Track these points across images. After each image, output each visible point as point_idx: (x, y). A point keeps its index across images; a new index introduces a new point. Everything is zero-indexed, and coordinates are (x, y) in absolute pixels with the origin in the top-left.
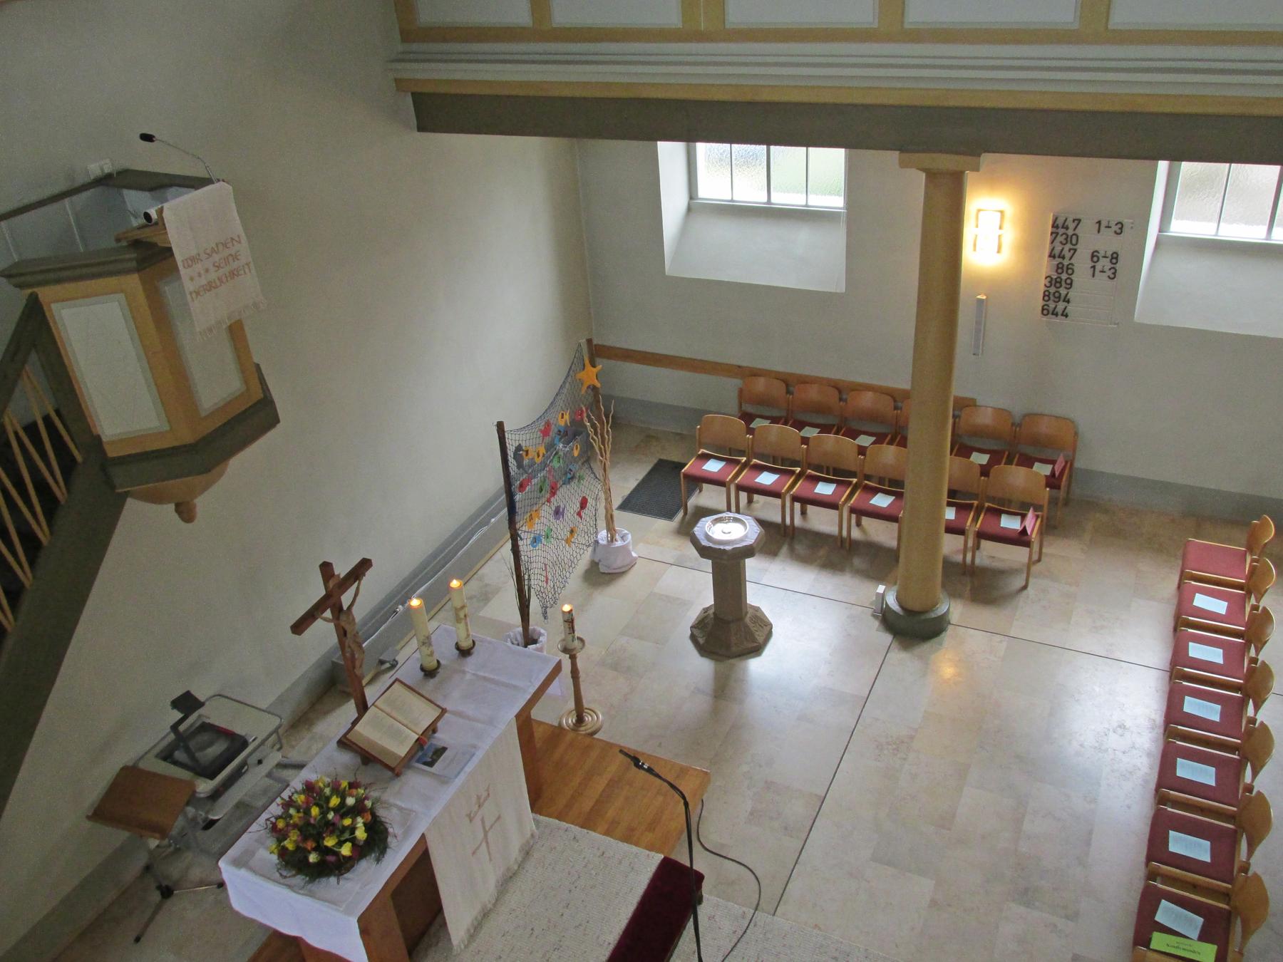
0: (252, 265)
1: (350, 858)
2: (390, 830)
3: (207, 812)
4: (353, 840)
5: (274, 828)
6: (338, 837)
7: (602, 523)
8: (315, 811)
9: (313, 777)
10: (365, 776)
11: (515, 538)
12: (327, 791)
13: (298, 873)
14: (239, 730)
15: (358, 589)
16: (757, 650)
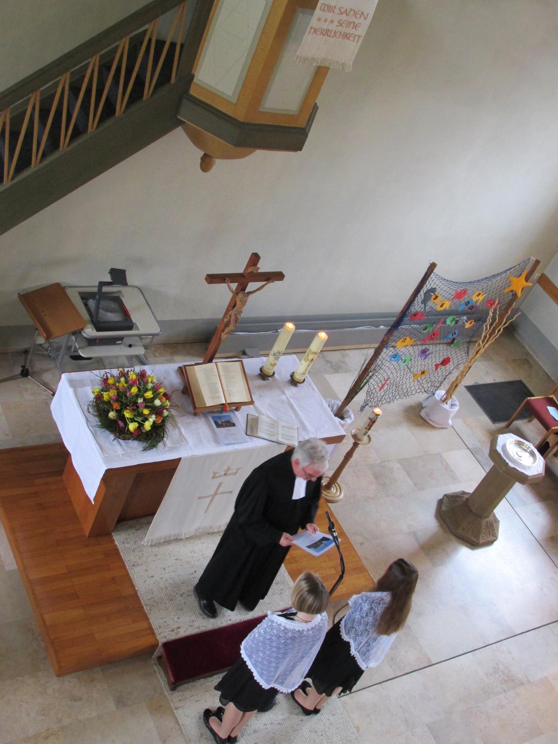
0: (361, 39)
1: (132, 433)
2: (165, 439)
3: (80, 348)
4: (141, 425)
5: (105, 380)
6: (135, 416)
7: (446, 385)
8: (134, 390)
9: (149, 373)
10: (177, 398)
12: (150, 386)
13: (97, 416)
14: (134, 318)
16: (474, 544)
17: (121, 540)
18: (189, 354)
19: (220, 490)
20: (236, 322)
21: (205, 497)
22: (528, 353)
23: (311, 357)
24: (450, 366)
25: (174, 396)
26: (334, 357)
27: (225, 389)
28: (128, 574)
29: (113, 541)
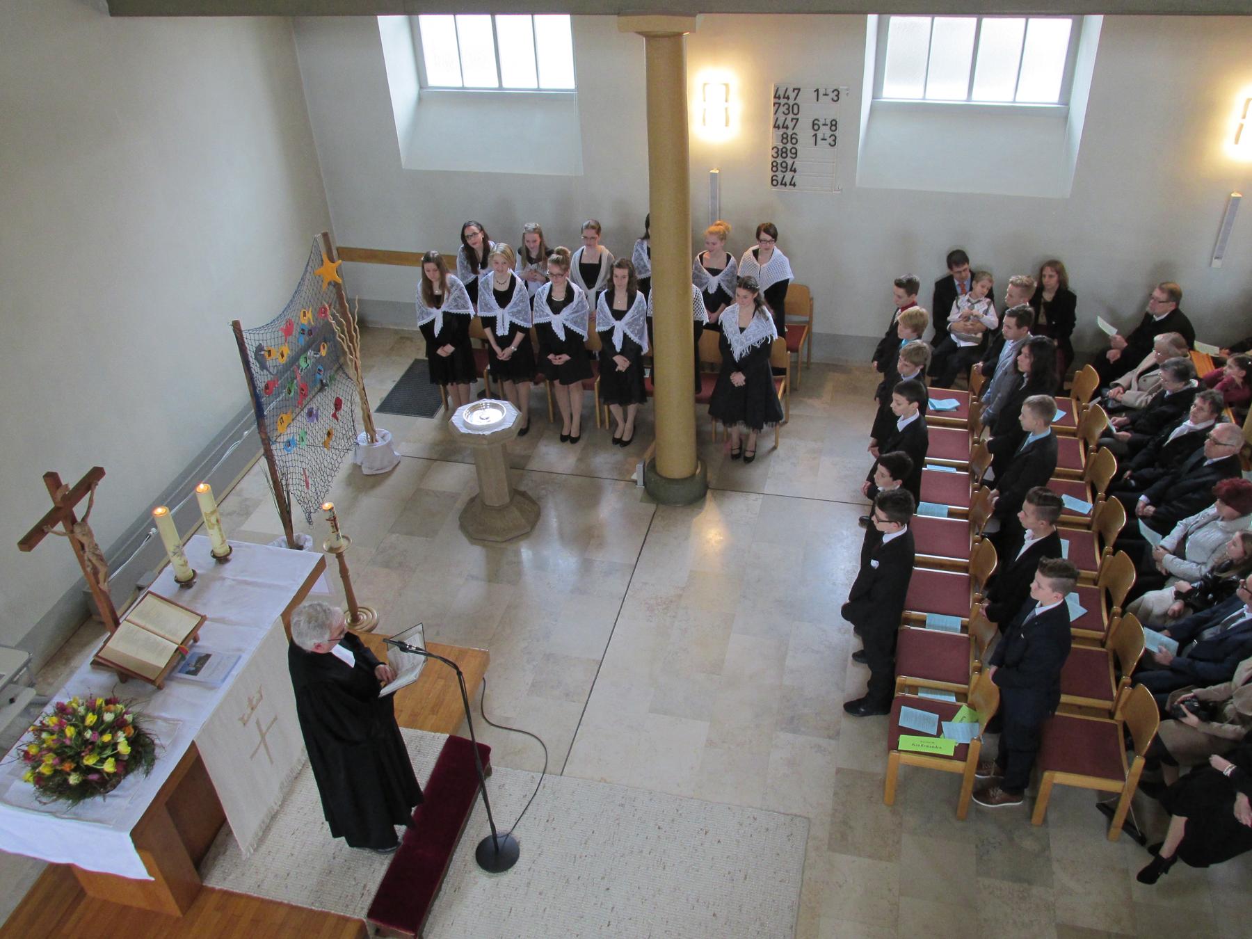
1: (115, 774)
2: (157, 742)
4: (117, 756)
5: (27, 755)
6: (100, 754)
7: (360, 426)
9: (66, 701)
10: (125, 692)
11: (269, 456)
12: (82, 710)
13: (59, 797)
15: (91, 500)
17: (221, 879)
18: (85, 644)
19: (264, 728)
20: (102, 560)
21: (256, 752)
22: (396, 332)
23: (213, 519)
24: (345, 407)
25: (117, 695)
26: (231, 503)
27: (162, 633)
28: (263, 901)
29: (213, 890)
